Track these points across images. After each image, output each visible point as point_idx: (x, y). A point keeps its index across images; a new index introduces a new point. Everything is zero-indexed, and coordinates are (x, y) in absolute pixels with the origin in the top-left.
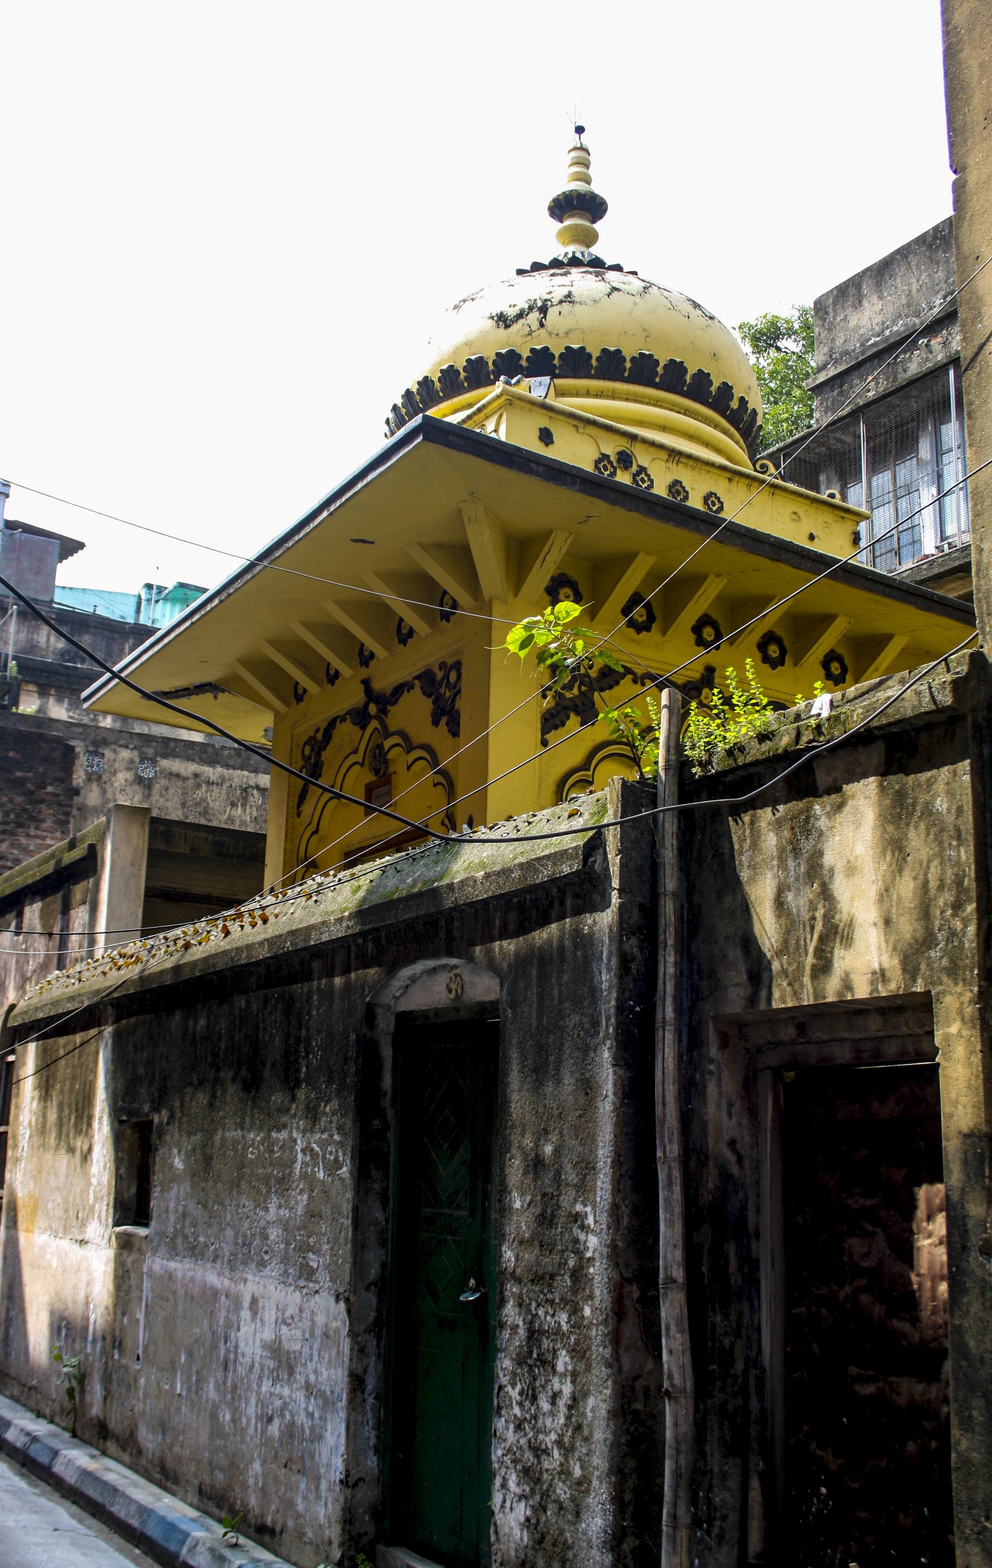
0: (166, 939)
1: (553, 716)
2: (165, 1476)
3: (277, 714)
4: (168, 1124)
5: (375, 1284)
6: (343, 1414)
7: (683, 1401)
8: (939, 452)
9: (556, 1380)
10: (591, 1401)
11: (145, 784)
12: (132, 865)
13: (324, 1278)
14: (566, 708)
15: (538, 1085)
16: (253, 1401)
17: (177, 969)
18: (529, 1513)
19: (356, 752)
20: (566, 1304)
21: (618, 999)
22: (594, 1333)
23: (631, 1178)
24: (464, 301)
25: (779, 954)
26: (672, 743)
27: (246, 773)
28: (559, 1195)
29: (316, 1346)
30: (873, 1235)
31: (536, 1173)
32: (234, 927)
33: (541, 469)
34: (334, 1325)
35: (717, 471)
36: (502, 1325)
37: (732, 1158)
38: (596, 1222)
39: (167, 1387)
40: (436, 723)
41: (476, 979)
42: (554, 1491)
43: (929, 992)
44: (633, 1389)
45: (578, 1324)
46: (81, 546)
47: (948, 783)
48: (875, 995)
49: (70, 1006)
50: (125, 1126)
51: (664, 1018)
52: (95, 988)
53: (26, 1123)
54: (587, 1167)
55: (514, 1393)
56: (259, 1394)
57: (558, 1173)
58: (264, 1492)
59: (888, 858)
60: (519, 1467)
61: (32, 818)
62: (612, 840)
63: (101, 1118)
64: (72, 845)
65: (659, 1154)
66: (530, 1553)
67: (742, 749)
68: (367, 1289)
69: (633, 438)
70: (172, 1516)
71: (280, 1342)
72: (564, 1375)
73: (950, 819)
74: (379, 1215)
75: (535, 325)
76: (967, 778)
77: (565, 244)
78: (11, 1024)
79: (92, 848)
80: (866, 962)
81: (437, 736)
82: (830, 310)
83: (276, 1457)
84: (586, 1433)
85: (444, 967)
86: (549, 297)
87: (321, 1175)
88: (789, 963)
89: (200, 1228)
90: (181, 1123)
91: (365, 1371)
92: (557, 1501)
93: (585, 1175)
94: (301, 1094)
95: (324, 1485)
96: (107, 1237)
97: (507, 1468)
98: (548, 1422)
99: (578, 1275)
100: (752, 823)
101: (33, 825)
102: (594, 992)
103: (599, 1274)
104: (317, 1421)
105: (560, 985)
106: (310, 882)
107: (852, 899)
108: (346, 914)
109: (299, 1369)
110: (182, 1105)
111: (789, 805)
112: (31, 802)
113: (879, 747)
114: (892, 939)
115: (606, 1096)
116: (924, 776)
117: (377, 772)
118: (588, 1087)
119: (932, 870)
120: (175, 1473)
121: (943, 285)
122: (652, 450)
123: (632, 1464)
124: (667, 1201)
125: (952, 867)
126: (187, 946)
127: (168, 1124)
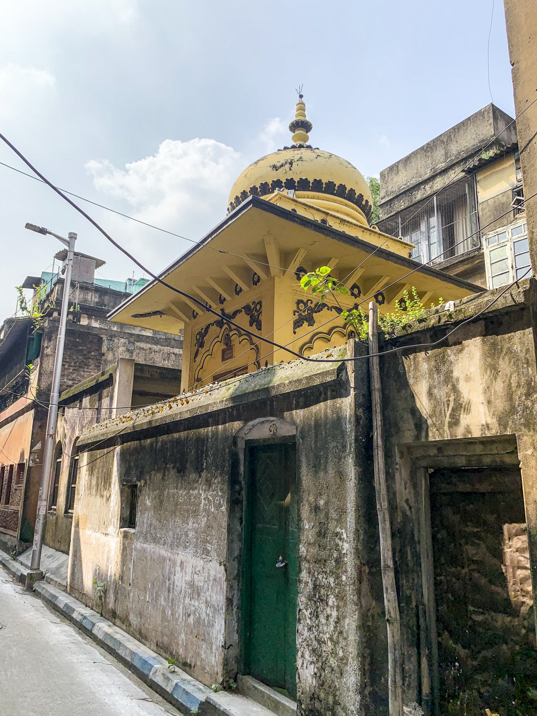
0: (144, 410)
1: (298, 322)
2: (141, 636)
3: (186, 323)
4: (144, 486)
5: (237, 558)
6: (223, 616)
7: (395, 624)
8: (429, 228)
9: (328, 609)
10: (347, 621)
11: (131, 352)
12: (127, 381)
13: (214, 554)
14: (303, 319)
15: (316, 472)
16: (181, 607)
17: (150, 422)
18: (316, 670)
19: (218, 337)
20: (333, 574)
21: (355, 436)
22: (348, 588)
23: (364, 517)
24: (259, 160)
25: (431, 417)
26: (375, 325)
27: (169, 348)
28: (328, 524)
29: (210, 585)
30: (479, 544)
31: (316, 512)
32: (174, 405)
33: (299, 220)
34: (219, 576)
35: (358, 228)
36: (300, 581)
37: (407, 508)
38: (347, 537)
39: (143, 598)
40: (251, 325)
41: (283, 426)
42: (329, 662)
43: (514, 434)
44: (367, 616)
45: (339, 584)
46: (104, 263)
47: (520, 338)
48: (484, 435)
49: (102, 438)
50: (125, 487)
51: (377, 445)
52: (113, 430)
53: (83, 485)
54: (342, 511)
55: (307, 613)
56: (184, 604)
57: (327, 514)
58: (186, 648)
59: (488, 373)
60: (310, 648)
61: (85, 365)
62: (350, 366)
63: (115, 483)
64: (103, 374)
65: (378, 507)
66: (317, 690)
67: (410, 326)
68: (234, 560)
69: (327, 214)
70: (145, 657)
71: (194, 581)
72: (332, 607)
73: (522, 355)
74: (239, 528)
75: (288, 170)
76: (531, 336)
77: (295, 141)
78: (77, 445)
79: (111, 375)
80: (478, 420)
81: (253, 330)
82: (386, 176)
83: (192, 633)
84: (345, 635)
85: (268, 421)
86: (293, 158)
87: (213, 510)
88: (436, 421)
89: (157, 530)
90: (149, 485)
91: (233, 596)
92: (330, 666)
93: (341, 515)
94: (204, 474)
95: (214, 647)
96: (117, 533)
97: (304, 648)
98: (325, 628)
99: (338, 561)
100: (415, 359)
101: (86, 367)
102: (343, 433)
103: (350, 562)
104: (211, 618)
105: (325, 429)
106: (207, 386)
107: (469, 392)
108: (225, 399)
109: (202, 594)
110: (150, 479)
111: (434, 351)
112: (85, 359)
113: (482, 322)
114: (492, 410)
115: (351, 479)
116: (506, 336)
117: (227, 344)
118: (341, 475)
119: (513, 378)
120: (146, 636)
121: (431, 165)
122: (334, 219)
123: (368, 651)
124: (384, 529)
125: (525, 377)
126: (153, 413)
127: (144, 486)
